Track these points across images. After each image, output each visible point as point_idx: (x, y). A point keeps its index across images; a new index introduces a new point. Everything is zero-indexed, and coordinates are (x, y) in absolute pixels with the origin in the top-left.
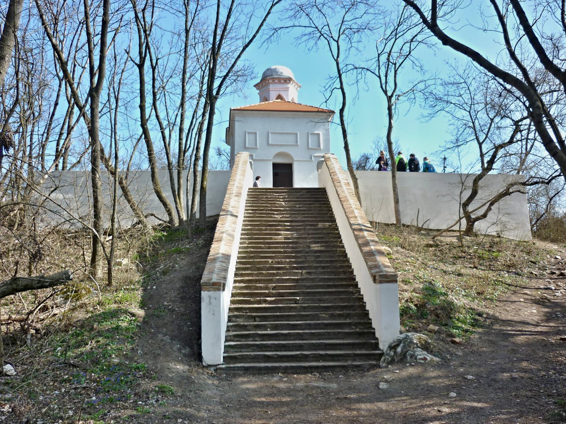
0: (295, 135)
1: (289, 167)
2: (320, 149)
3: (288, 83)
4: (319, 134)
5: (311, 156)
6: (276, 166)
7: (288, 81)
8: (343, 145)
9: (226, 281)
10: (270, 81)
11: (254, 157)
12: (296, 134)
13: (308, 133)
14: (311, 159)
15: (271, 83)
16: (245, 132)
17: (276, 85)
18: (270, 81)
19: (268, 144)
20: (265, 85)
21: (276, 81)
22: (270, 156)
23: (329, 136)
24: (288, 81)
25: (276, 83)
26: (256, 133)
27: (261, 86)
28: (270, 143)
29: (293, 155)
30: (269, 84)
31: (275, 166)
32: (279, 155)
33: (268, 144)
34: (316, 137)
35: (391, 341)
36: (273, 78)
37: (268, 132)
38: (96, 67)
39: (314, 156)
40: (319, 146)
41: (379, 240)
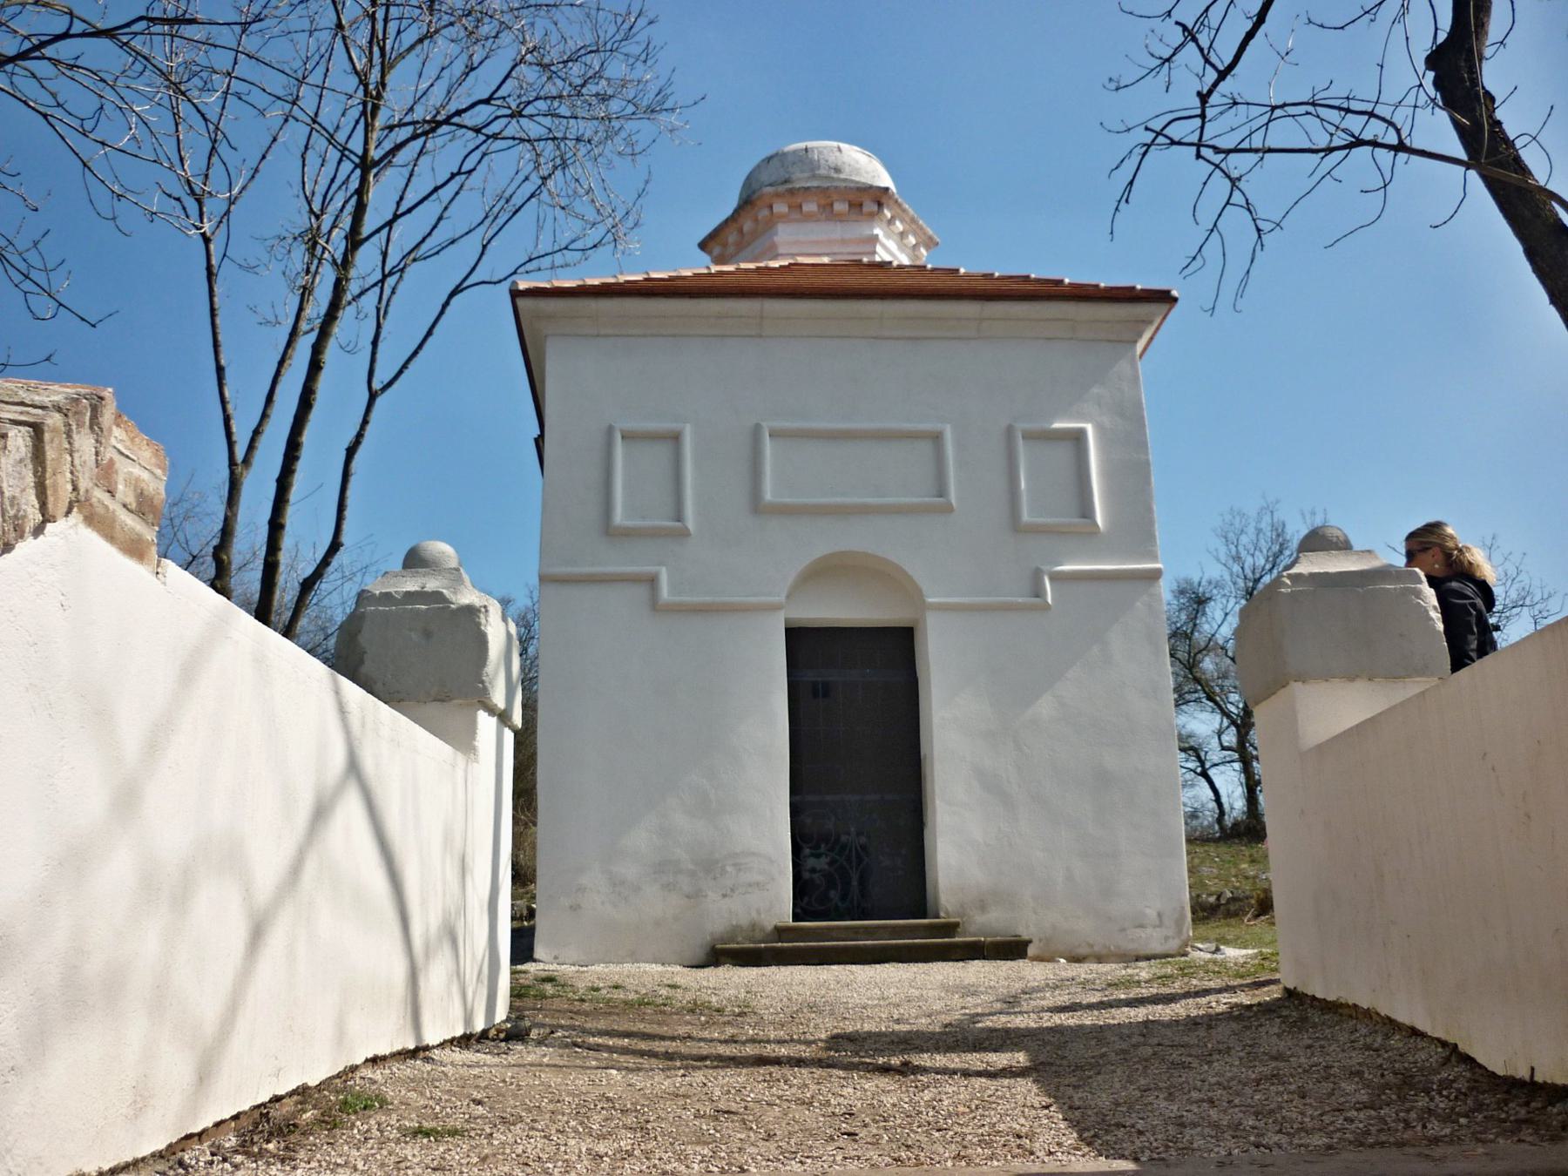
0: (925, 447)
1: (898, 645)
3: (872, 216)
4: (1078, 437)
5: (1037, 576)
7: (870, 207)
8: (430, 339)
10: (780, 208)
11: (665, 593)
12: (937, 438)
13: (1009, 432)
14: (1038, 592)
15: (783, 218)
17: (811, 226)
18: (780, 208)
19: (757, 506)
20: (755, 235)
21: (810, 207)
22: (772, 589)
23: (1142, 445)
24: (870, 207)
25: (809, 217)
26: (676, 438)
27: (732, 238)
28: (768, 495)
29: (917, 571)
30: (771, 223)
32: (826, 571)
33: (757, 506)
34: (1061, 454)
35: (744, 921)
36: (792, 192)
37: (756, 431)
39: (1057, 578)
40: (1086, 511)
41: (1330, 1135)
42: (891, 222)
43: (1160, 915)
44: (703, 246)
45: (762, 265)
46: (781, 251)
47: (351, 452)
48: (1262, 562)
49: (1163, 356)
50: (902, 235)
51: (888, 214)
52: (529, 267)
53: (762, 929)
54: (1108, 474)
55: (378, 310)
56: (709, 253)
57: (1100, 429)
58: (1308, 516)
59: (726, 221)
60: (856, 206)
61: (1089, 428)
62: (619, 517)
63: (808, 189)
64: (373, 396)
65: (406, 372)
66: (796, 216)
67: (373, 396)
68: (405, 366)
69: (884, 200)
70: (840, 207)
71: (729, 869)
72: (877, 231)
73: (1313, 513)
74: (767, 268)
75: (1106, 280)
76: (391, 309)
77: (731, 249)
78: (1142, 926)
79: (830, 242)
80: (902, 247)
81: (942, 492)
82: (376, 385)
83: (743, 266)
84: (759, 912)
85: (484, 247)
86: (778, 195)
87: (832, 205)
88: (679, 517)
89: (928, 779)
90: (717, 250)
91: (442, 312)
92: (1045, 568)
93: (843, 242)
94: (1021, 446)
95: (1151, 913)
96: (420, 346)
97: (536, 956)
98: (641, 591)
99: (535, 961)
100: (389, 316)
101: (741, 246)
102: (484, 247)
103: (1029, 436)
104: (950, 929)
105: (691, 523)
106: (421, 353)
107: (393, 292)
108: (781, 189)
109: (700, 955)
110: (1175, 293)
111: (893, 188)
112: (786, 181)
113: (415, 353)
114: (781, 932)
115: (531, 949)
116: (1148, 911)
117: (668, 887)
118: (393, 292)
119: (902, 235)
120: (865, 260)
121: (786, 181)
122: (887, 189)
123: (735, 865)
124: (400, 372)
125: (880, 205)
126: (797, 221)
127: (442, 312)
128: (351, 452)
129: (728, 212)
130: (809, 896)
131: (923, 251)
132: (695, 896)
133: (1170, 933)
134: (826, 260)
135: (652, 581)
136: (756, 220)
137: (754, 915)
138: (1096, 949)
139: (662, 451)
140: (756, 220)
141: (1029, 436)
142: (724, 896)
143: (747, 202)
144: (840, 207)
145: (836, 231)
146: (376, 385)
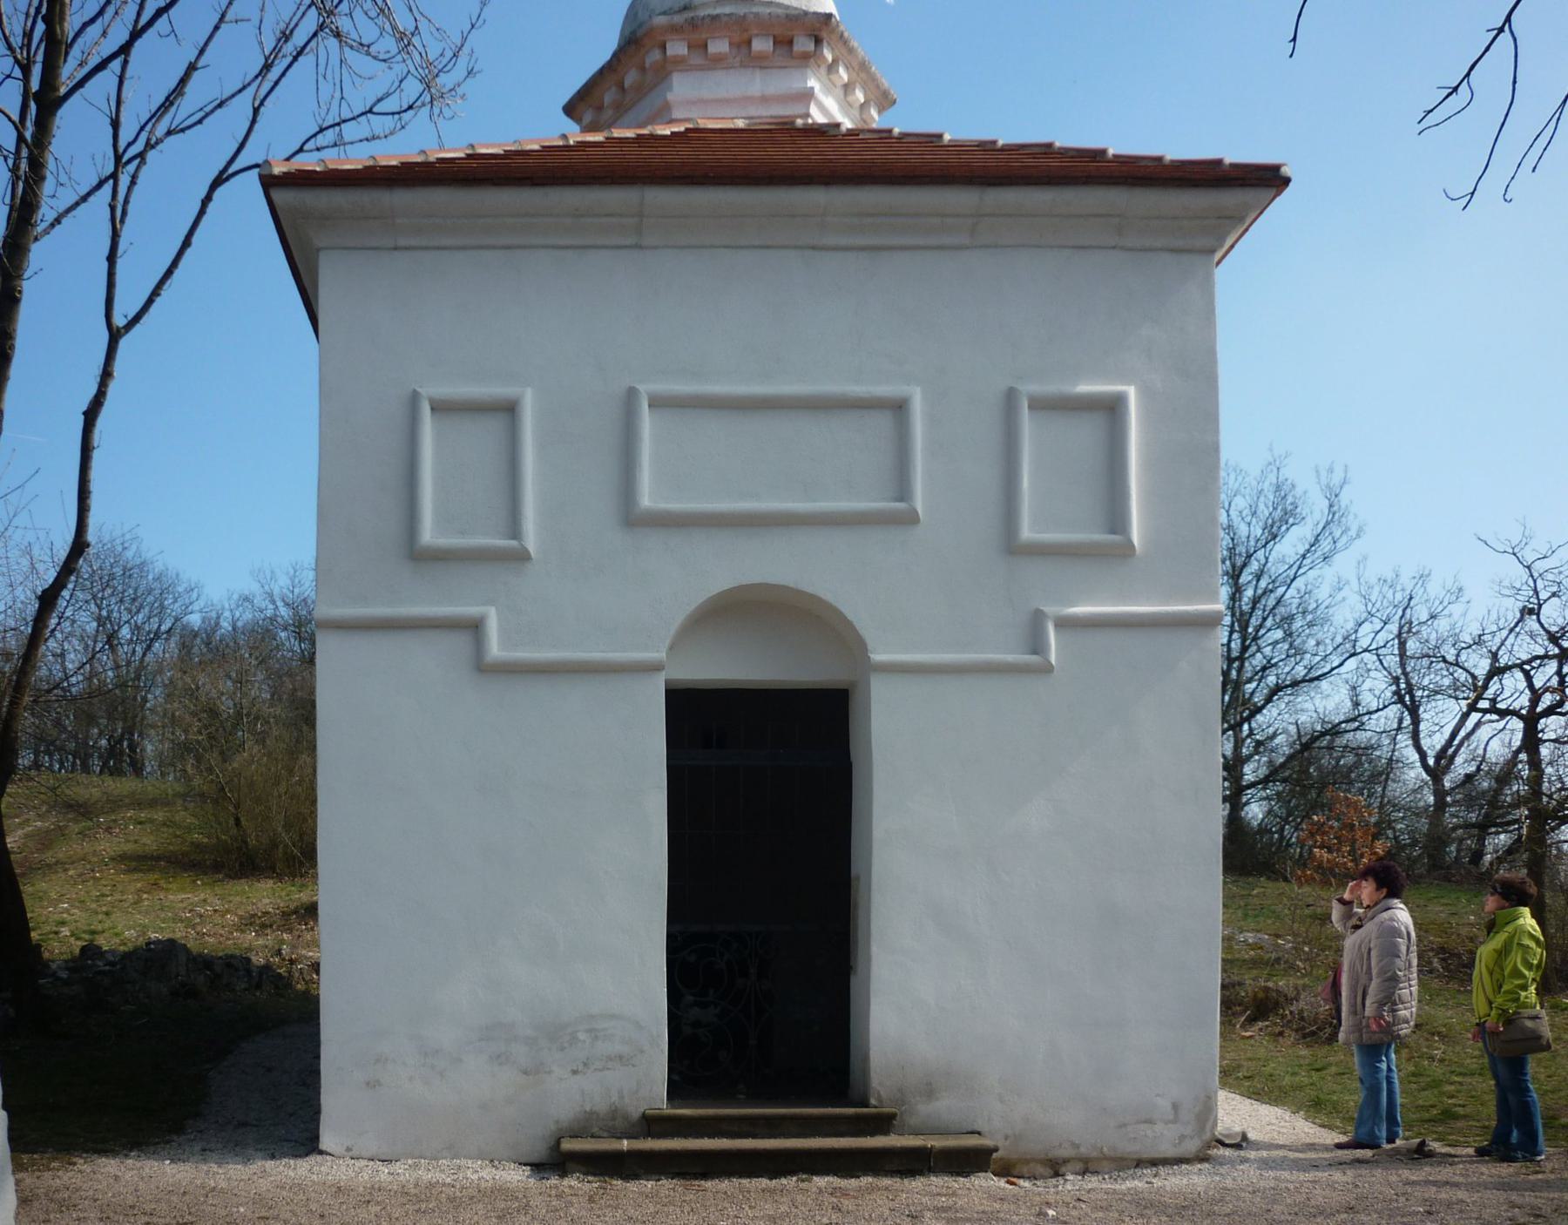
2: (1126, 550)
3: (805, 58)
4: (1112, 408)
5: (1038, 618)
6: (694, 715)
7: (803, 44)
8: (189, 252)
9: (318, 973)
10: (677, 48)
11: (495, 649)
12: (899, 408)
13: (1011, 396)
14: (1037, 645)
15: (679, 62)
16: (415, 398)
18: (677, 48)
20: (642, 91)
21: (719, 46)
24: (803, 44)
25: (717, 62)
26: (509, 409)
31: (687, 708)
35: (601, 1106)
36: (694, 24)
38: (1456, 742)
39: (1064, 624)
42: (832, 68)
43: (1175, 1107)
44: (570, 110)
45: (645, 131)
46: (676, 114)
47: (91, 415)
48: (1259, 532)
49: (1256, 272)
50: (848, 88)
51: (828, 55)
52: (321, 140)
53: (626, 1117)
54: (1148, 464)
55: (113, 208)
56: (578, 120)
57: (1146, 393)
58: (1323, 473)
59: (602, 72)
60: (784, 43)
61: (1131, 392)
62: (429, 535)
63: (715, 18)
64: (115, 336)
65: (158, 300)
66: (697, 60)
67: (115, 336)
68: (155, 293)
69: (824, 34)
70: (761, 45)
71: (582, 1036)
72: (812, 83)
73: (1331, 470)
74: (653, 137)
75: (1176, 149)
76: (130, 208)
77: (608, 114)
78: (1150, 1121)
79: (748, 100)
80: (846, 105)
81: (903, 491)
82: (119, 321)
83: (617, 133)
84: (621, 1097)
85: (256, 111)
86: (675, 29)
87: (749, 42)
88: (515, 531)
89: (861, 921)
90: (588, 117)
91: (202, 212)
92: (1051, 609)
93: (764, 100)
94: (1027, 422)
95: (1164, 1104)
96: (175, 263)
97: (323, 1146)
98: (460, 643)
99: (321, 1153)
100: (128, 219)
101: (621, 111)
102: (256, 111)
103: (1041, 405)
104: (883, 1123)
105: (531, 542)
106: (177, 273)
107: (133, 182)
108: (678, 19)
109: (539, 1151)
110: (1286, 171)
111: (835, 12)
112: (685, 8)
113: (169, 273)
114: (652, 1124)
115: (315, 1138)
116: (1159, 1101)
117: (500, 1059)
118: (133, 182)
119: (848, 88)
120: (799, 122)
121: (685, 8)
122: (829, 16)
123: (589, 1031)
124: (150, 302)
125: (818, 41)
126: (701, 68)
127: (202, 212)
128: (91, 415)
129: (605, 56)
130: (693, 1061)
131: (874, 113)
132: (534, 1071)
133: (1188, 1131)
134: (741, 124)
135: (475, 627)
136: (643, 69)
137: (615, 1098)
138: (1083, 1150)
139: (493, 426)
140: (643, 69)
141: (1041, 405)
142: (575, 1072)
143: (633, 42)
144: (761, 45)
145: (756, 84)
146: (119, 321)
